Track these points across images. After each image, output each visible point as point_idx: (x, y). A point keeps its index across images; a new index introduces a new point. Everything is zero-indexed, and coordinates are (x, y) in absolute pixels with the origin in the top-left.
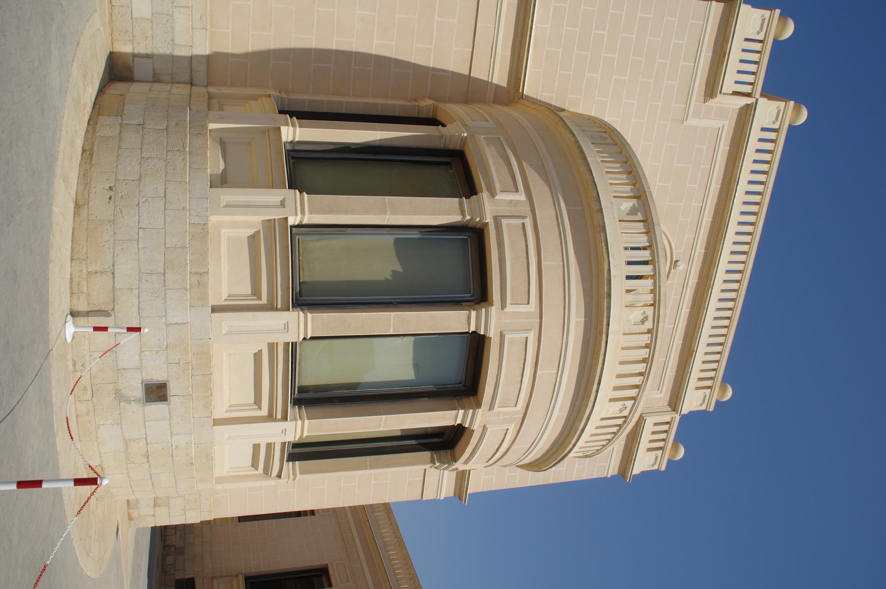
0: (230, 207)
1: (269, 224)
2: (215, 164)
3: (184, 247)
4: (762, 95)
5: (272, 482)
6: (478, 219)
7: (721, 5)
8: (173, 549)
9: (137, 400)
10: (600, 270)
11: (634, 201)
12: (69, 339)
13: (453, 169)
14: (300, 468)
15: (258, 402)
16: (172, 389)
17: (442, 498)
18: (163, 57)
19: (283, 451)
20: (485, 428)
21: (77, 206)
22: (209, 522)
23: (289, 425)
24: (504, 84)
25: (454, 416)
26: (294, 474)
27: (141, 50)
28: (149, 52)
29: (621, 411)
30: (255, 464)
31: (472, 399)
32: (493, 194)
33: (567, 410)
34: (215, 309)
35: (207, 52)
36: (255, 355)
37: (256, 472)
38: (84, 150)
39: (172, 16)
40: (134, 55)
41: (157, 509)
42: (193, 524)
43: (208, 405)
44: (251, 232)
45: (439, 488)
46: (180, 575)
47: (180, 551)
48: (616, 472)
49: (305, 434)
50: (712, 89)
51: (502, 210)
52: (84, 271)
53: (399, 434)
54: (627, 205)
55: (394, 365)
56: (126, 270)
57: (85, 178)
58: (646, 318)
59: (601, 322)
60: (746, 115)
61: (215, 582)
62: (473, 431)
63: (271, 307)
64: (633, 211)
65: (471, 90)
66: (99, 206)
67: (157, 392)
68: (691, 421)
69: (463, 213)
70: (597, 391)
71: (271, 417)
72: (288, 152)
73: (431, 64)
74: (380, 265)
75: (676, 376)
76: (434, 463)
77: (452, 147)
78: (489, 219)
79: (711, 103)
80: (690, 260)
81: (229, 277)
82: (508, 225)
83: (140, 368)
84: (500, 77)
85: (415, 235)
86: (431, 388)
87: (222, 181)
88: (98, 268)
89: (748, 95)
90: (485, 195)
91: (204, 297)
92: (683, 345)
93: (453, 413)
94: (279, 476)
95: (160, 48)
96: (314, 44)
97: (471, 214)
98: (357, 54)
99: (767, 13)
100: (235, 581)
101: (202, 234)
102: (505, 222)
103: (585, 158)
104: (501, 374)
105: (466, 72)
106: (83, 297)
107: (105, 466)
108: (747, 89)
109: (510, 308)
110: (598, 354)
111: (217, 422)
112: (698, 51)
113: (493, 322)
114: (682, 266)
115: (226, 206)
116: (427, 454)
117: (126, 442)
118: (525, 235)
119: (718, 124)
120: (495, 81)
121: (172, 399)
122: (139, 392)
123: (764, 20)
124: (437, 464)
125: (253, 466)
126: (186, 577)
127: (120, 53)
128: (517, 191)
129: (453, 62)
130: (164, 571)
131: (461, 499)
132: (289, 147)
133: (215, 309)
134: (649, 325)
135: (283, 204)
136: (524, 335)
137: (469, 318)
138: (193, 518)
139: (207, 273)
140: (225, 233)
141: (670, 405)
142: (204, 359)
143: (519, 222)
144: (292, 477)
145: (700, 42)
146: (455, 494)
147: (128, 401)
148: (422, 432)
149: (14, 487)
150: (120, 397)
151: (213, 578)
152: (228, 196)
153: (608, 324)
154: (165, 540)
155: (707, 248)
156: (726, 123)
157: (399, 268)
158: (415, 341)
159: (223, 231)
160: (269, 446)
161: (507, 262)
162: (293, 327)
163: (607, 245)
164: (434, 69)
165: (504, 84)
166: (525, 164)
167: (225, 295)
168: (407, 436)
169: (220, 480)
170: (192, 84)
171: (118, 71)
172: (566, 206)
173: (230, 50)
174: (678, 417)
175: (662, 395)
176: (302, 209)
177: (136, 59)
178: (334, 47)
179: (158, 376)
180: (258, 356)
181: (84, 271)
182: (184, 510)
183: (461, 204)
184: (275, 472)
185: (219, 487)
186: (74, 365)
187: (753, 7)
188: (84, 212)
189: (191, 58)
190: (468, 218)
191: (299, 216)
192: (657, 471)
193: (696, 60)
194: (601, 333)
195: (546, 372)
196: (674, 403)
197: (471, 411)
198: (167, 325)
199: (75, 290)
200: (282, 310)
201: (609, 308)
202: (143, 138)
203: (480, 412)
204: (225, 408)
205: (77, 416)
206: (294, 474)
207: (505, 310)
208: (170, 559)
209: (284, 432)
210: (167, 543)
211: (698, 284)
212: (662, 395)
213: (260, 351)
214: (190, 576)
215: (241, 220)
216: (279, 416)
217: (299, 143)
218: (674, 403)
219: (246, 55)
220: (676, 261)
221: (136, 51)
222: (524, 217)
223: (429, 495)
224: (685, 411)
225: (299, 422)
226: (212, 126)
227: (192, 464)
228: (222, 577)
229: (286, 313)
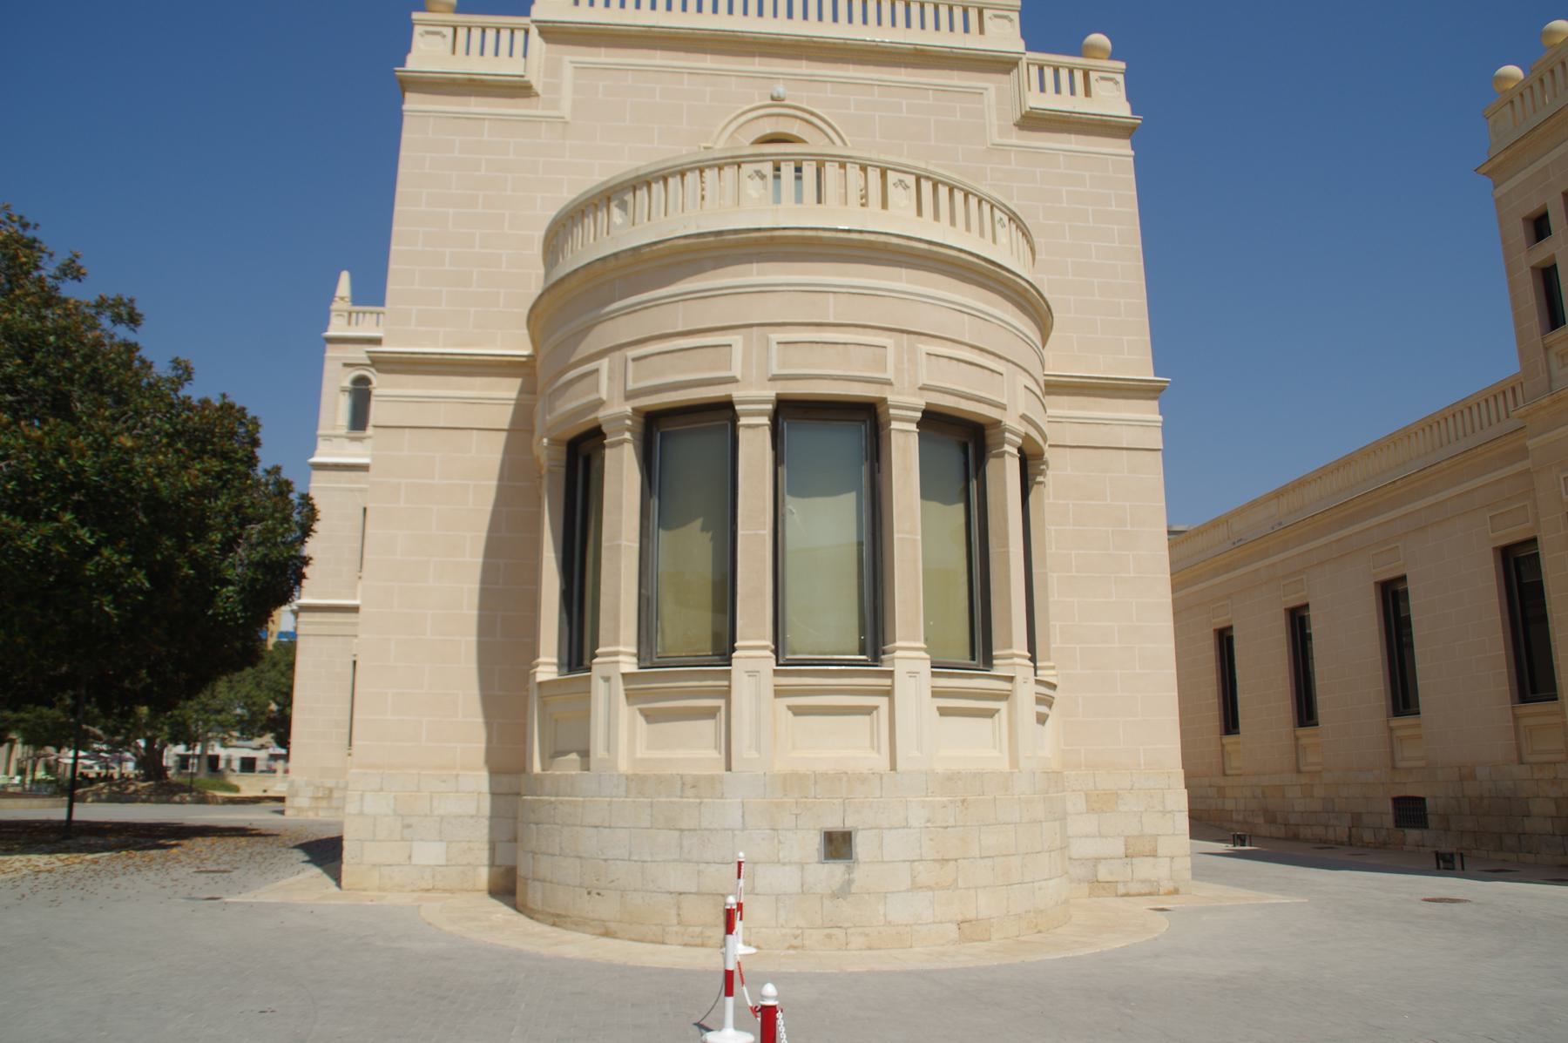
0: (610, 746)
1: (631, 697)
3: (652, 805)
4: (527, 14)
6: (629, 422)
7: (408, 96)
9: (849, 870)
10: (688, 249)
11: (613, 205)
12: (752, 950)
13: (583, 451)
14: (1004, 648)
15: (868, 711)
16: (835, 824)
18: (492, 828)
20: (923, 388)
21: (607, 934)
22: (1186, 777)
24: (517, 382)
25: (902, 435)
26: (1011, 656)
27: (484, 856)
28: (486, 847)
29: (907, 187)
30: (990, 714)
31: (880, 410)
32: (600, 404)
33: (897, 270)
34: (729, 768)
35: (484, 774)
36: (795, 714)
38: (554, 925)
39: (442, 818)
40: (492, 864)
41: (1160, 852)
42: (1189, 797)
44: (640, 720)
45: (1144, 424)
46: (1389, 820)
47: (1356, 819)
48: (1127, 142)
50: (519, 89)
51: (619, 393)
52: (675, 929)
54: (617, 216)
55: (826, 524)
56: (677, 878)
57: (579, 924)
58: (758, 172)
59: (756, 240)
60: (555, 34)
63: (726, 694)
64: (623, 206)
65: (522, 426)
66: (605, 908)
67: (838, 845)
68: (1035, 36)
69: (621, 443)
70: (861, 232)
71: (889, 693)
72: (571, 670)
73: (494, 483)
74: (690, 546)
75: (663, 48)
77: (563, 457)
78: (628, 408)
79: (538, 86)
80: (770, 78)
81: (689, 748)
82: (635, 381)
83: (802, 865)
84: (508, 389)
85: (655, 503)
86: (865, 469)
87: (585, 754)
88: (673, 912)
89: (527, 32)
90: (602, 414)
91: (712, 780)
92: (907, 66)
94: (1011, 679)
95: (482, 832)
96: (472, 638)
97: (621, 432)
98: (483, 581)
99: (418, 30)
100: (1399, 733)
101: (637, 782)
102: (631, 386)
103: (568, 275)
104: (831, 373)
105: (504, 435)
106: (708, 932)
107: (960, 918)
108: (519, 36)
109: (736, 371)
110: (804, 238)
111: (893, 767)
112: (469, 118)
113: (754, 393)
114: (780, 89)
116: (992, 466)
117: (915, 887)
118: (645, 357)
119: (568, 70)
120: (514, 394)
121: (849, 825)
122: (837, 868)
123: (428, 33)
126: (1390, 809)
127: (490, 881)
128: (597, 371)
129: (488, 454)
130: (1382, 846)
131: (1162, 389)
132: (565, 670)
133: (729, 768)
135: (607, 679)
136: (774, 347)
137: (749, 426)
139: (682, 777)
140: (641, 753)
141: (1008, 72)
142: (793, 782)
143: (630, 365)
145: (457, 117)
147: (850, 882)
149: (730, 1000)
150: (843, 891)
151: (1394, 768)
152: (598, 750)
153: (759, 230)
154: (1342, 844)
155: (752, 54)
156: (567, 58)
157: (699, 523)
158: (794, 494)
159: (639, 755)
160: (936, 694)
161: (678, 378)
162: (752, 664)
163: (655, 243)
164: (501, 478)
165: (517, 382)
166: (573, 360)
167: (714, 754)
169: (1014, 761)
171: (506, 888)
172: (614, 301)
173: (482, 745)
174: (1030, 55)
175: (992, 87)
176: (619, 653)
177: (498, 862)
178: (475, 612)
179: (815, 842)
180: (797, 711)
181: (675, 929)
182: (1164, 813)
183: (613, 445)
186: (795, 948)
187: (409, 51)
188: (613, 926)
189: (493, 794)
190: (627, 435)
191: (621, 658)
192: (1126, 75)
193: (479, 118)
194: (772, 238)
195: (832, 309)
196: (1003, 65)
197: (892, 411)
198: (744, 829)
199: (699, 941)
200: (729, 679)
201: (736, 231)
202: (543, 853)
203: (892, 398)
204: (874, 755)
205: (870, 948)
207: (739, 377)
208: (1368, 836)
209: (913, 674)
210: (1346, 839)
211: (809, 59)
212: (992, 87)
213: (789, 708)
214: (1390, 803)
215: (626, 735)
216: (888, 682)
217: (560, 658)
218: (1003, 65)
219: (489, 725)
220: (773, 99)
221: (485, 861)
223: (1155, 439)
224: (1019, 46)
225: (898, 654)
226: (537, 767)
227: (964, 801)
228: (1392, 752)
229: (734, 675)
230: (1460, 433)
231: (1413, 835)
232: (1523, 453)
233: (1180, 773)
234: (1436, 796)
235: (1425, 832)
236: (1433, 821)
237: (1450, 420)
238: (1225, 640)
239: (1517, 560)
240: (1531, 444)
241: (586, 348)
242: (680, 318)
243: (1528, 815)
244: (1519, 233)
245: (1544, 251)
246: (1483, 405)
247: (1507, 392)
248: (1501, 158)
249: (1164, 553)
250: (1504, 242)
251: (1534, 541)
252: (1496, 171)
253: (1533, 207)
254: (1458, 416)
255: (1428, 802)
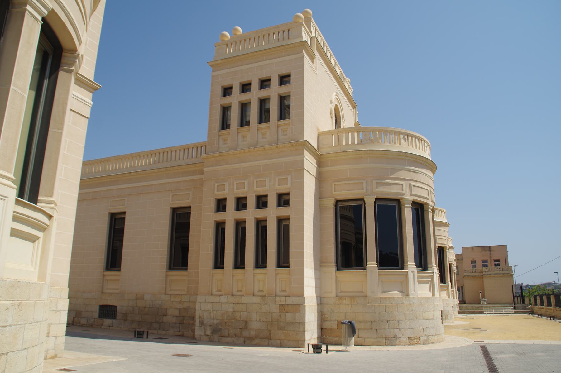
2: (396, 294)
5: (54, 225)
8: (76, 318)
17: (92, 103)
19: (25, 205)
23: (410, 275)
26: (51, 202)
30: (32, 239)
32: (404, 194)
37: (41, 240)
43: (428, 299)
46: (96, 315)
49: (11, 176)
53: (33, 93)
61: (105, 291)
62: (53, 9)
76: (72, 71)
90: (403, 197)
93: (27, 19)
94: (50, 217)
115: (415, 291)
116: (62, 75)
124: (74, 68)
125: (34, 242)
126: (98, 310)
131: (96, 89)
134: (406, 137)
138: (64, 304)
144: (53, 205)
146: (91, 92)
148: (37, 74)
151: (102, 292)
160: (17, 218)
168: (37, 87)
169: (42, 276)
170: (321, 304)
182: (56, 311)
184: (45, 219)
185: (48, 279)
197: (28, 8)
206: (51, 202)
208: (83, 321)
209: (413, 272)
214: (98, 308)
222: (410, 184)
223: (87, 112)
227: (19, 304)
228: (103, 286)
230: (165, 160)
231: (108, 322)
232: (201, 172)
233: (67, 290)
234: (121, 305)
235: (114, 321)
236: (119, 316)
237: (162, 154)
238: (117, 224)
239: (115, 219)
240: (205, 169)
241: (395, 175)
242: (421, 178)
243: (166, 315)
244: (219, 92)
245: (227, 100)
246: (178, 152)
247: (199, 147)
248: (219, 62)
249: (79, 171)
250: (212, 92)
251: (190, 207)
252: (215, 66)
253: (227, 83)
254: (166, 154)
255: (119, 309)
